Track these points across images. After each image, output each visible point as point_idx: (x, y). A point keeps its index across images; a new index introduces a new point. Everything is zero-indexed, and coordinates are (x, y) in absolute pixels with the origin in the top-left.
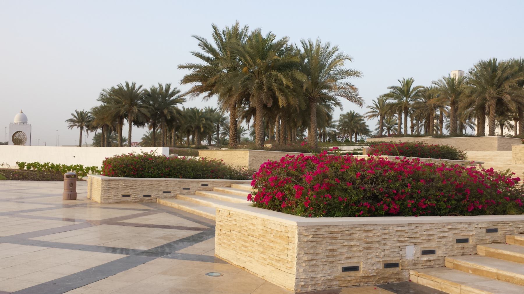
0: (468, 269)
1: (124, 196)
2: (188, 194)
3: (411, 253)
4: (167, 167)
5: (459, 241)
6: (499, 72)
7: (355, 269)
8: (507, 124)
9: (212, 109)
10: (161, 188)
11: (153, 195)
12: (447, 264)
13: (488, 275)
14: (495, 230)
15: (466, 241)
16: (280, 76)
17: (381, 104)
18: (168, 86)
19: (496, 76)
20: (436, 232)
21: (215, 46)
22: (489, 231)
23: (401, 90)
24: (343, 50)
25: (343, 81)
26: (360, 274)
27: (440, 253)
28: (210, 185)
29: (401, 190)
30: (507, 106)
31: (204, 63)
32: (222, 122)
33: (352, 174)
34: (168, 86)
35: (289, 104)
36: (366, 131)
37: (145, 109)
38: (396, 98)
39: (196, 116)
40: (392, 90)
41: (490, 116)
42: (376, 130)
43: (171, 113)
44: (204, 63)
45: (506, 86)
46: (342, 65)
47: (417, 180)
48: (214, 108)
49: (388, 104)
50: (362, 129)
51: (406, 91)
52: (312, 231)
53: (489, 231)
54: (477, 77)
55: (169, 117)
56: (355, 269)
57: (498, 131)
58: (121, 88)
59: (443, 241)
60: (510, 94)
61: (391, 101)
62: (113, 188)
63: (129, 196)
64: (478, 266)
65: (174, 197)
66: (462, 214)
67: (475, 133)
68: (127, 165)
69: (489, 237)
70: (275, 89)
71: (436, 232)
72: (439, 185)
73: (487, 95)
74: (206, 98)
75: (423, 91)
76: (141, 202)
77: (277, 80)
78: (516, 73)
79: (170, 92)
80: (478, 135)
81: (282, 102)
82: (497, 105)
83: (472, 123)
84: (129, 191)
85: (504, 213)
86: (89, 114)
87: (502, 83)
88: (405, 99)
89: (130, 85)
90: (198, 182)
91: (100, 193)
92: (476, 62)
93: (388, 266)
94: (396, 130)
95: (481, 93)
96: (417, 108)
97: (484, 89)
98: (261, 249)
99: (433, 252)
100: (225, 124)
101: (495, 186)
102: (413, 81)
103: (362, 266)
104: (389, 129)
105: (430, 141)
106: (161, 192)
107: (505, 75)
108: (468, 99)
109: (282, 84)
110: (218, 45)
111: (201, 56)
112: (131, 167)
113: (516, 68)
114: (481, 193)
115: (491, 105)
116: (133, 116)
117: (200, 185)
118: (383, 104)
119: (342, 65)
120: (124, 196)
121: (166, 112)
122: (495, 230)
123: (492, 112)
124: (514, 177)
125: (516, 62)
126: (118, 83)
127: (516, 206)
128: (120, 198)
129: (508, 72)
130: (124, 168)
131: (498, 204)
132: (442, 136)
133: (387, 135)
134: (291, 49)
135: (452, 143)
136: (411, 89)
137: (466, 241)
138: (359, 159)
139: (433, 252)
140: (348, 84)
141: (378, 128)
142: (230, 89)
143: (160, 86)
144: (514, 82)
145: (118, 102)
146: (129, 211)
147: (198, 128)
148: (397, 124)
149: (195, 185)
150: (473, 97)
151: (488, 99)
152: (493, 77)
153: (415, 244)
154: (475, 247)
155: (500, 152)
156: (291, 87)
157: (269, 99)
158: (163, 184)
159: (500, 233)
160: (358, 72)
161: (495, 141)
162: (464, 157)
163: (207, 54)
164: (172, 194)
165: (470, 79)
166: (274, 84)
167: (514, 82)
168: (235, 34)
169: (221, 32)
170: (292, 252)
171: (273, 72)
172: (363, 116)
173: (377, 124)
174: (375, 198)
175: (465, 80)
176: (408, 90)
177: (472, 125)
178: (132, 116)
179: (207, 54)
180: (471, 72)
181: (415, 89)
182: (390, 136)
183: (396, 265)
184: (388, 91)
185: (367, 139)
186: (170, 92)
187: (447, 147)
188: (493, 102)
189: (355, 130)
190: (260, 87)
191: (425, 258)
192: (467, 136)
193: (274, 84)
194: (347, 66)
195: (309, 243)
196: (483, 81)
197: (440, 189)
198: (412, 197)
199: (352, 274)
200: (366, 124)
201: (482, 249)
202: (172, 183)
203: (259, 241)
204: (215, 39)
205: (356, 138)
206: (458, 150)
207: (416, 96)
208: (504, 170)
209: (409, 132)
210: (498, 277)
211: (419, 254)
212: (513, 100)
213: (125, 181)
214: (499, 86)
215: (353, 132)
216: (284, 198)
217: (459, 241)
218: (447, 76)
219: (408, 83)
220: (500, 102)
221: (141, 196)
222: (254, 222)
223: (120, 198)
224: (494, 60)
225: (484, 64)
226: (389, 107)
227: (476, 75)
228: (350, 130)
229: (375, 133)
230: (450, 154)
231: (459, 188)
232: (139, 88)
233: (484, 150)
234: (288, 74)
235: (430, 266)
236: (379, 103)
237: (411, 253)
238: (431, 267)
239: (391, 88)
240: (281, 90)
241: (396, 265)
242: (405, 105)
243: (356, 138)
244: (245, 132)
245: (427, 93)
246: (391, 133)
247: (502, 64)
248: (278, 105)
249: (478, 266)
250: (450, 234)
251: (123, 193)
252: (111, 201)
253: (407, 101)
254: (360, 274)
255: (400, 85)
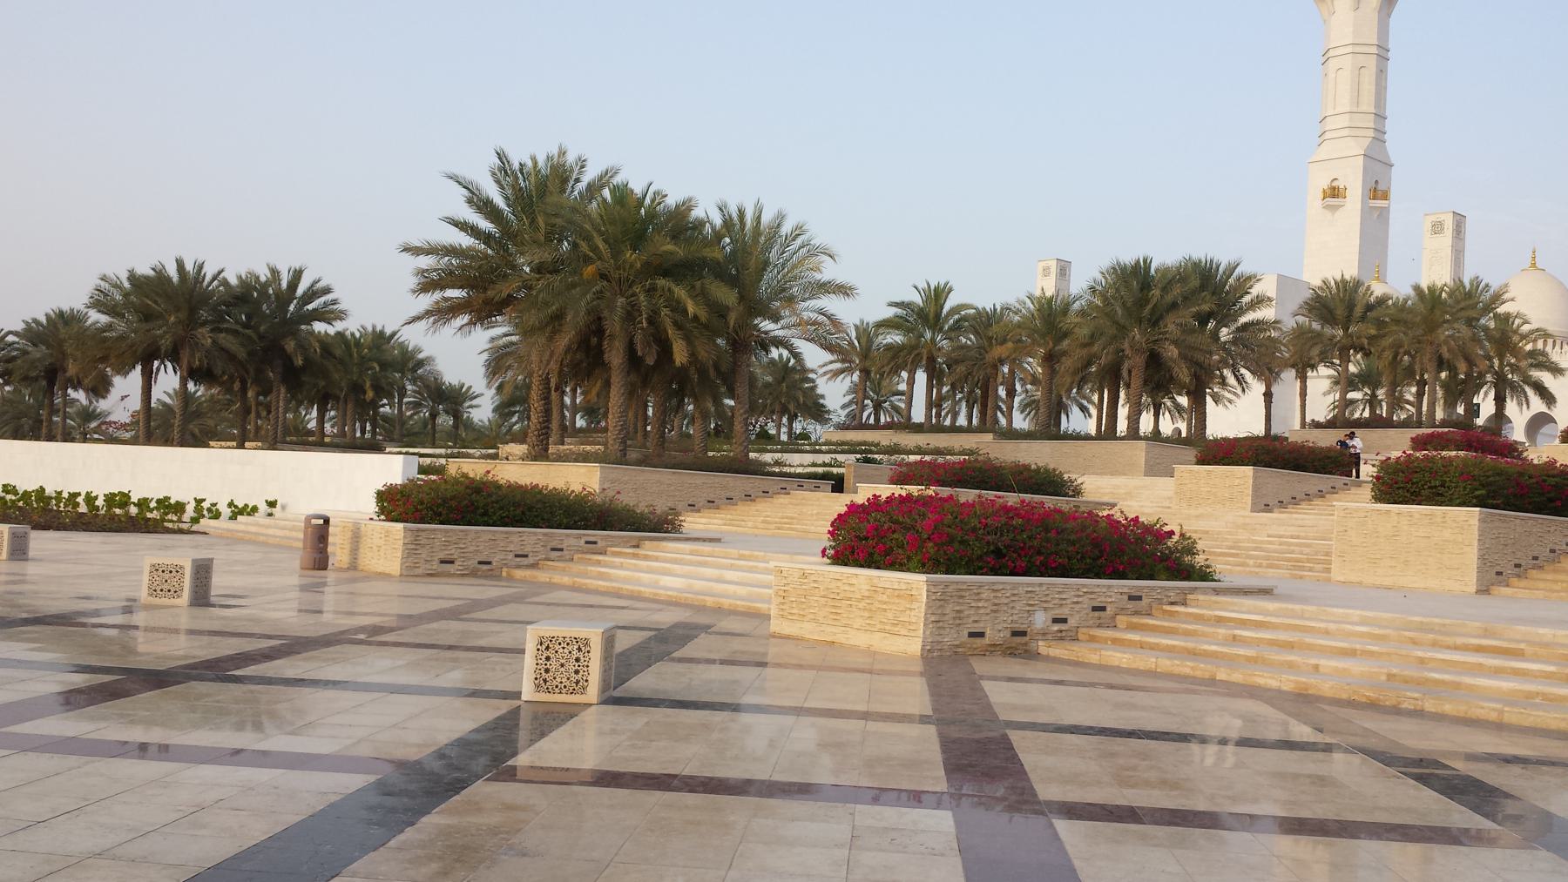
0: (1106, 640)
1: (442, 562)
2: (560, 559)
3: (1040, 620)
4: (517, 505)
5: (1095, 609)
6: (1156, 292)
7: (982, 635)
8: (1169, 403)
9: (382, 333)
10: (511, 547)
11: (496, 560)
12: (1081, 636)
13: (1131, 644)
14: (1139, 598)
15: (1103, 609)
16: (680, 292)
17: (864, 340)
18: (297, 275)
19: (1147, 301)
20: (1070, 596)
21: (500, 202)
22: (1131, 598)
23: (921, 314)
24: (819, 234)
25: (810, 308)
26: (986, 641)
27: (1072, 622)
28: (601, 544)
29: (1029, 544)
30: (1170, 370)
31: (465, 241)
32: (414, 370)
33: (974, 522)
34: (297, 275)
35: (693, 355)
36: (817, 411)
37: (230, 338)
38: (908, 331)
39: (351, 355)
40: (899, 311)
41: (1132, 391)
42: (844, 407)
43: (302, 347)
44: (465, 241)
45: (1171, 325)
46: (818, 270)
47: (1047, 530)
48: (388, 332)
49: (889, 347)
50: (810, 404)
51: (931, 316)
52: (939, 589)
53: (1131, 598)
54: (1105, 299)
55: (299, 362)
56: (982, 635)
57: (1146, 423)
58: (160, 276)
59: (1077, 607)
60: (1175, 343)
61: (895, 338)
62: (423, 546)
63: (452, 562)
64: (1118, 635)
65: (534, 566)
66: (1098, 576)
67: (1091, 427)
68: (445, 501)
69: (1131, 605)
70: (668, 323)
71: (1070, 596)
72: (1073, 537)
73: (1126, 346)
74: (467, 329)
75: (974, 318)
76: (473, 574)
77: (678, 308)
78: (1194, 292)
79: (300, 291)
80: (1100, 437)
81: (680, 355)
82: (1147, 366)
83: (1084, 397)
84: (453, 552)
85: (1151, 578)
86: (10, 338)
87: (1161, 317)
88: (928, 335)
89: (189, 267)
90: (579, 537)
91: (399, 554)
92: (1106, 262)
93: (1015, 634)
94: (896, 409)
95: (1114, 338)
96: (957, 362)
97: (1123, 330)
98: (866, 614)
99: (1064, 621)
100: (421, 377)
101: (1140, 540)
102: (950, 290)
103: (988, 632)
104: (878, 407)
105: (987, 446)
106: (511, 556)
107: (1169, 298)
108: (1085, 352)
109: (685, 311)
110: (507, 198)
111: (456, 224)
112: (454, 504)
113: (1195, 282)
114: (1122, 550)
115: (1134, 364)
116: (198, 355)
117: (582, 542)
118: (870, 341)
119: (818, 270)
120: (442, 562)
121: (290, 345)
122: (1139, 598)
123: (1136, 382)
124: (1166, 529)
125: (1197, 265)
126: (154, 262)
127: (1167, 569)
128: (435, 566)
129: (1177, 291)
130: (439, 506)
131: (1144, 565)
132: (1012, 434)
133: (872, 421)
134: (700, 224)
135: (1037, 455)
136: (945, 311)
137: (1103, 609)
138: (962, 500)
139: (1064, 621)
140: (821, 312)
141: (851, 402)
142: (558, 317)
143: (275, 272)
144: (1186, 316)
145: (147, 316)
146: (162, 624)
147: (357, 389)
148: (902, 393)
149: (573, 541)
150: (1095, 348)
151: (1128, 352)
152: (1142, 302)
153: (1045, 609)
154: (1113, 618)
155: (1149, 480)
156: (703, 320)
157: (649, 344)
158: (515, 539)
159: (1145, 601)
160: (851, 288)
161: (1139, 450)
162: (1077, 492)
163: (485, 225)
164: (530, 560)
165: (1090, 303)
166: (665, 311)
167: (1186, 316)
168: (560, 174)
169: (516, 166)
170: (918, 612)
171: (661, 282)
172: (812, 371)
173: (848, 393)
174: (998, 553)
175: (1076, 306)
176: (938, 315)
177: (1085, 403)
178: (193, 355)
179: (485, 225)
180: (1093, 290)
181: (954, 311)
182: (877, 426)
183: (1024, 634)
184: (891, 312)
185: (818, 431)
186: (300, 291)
187: (1047, 470)
188: (1140, 361)
189: (791, 407)
190: (630, 315)
191: (1056, 627)
192: (1077, 437)
193: (665, 311)
194: (829, 272)
195: (938, 601)
196: (1120, 312)
197: (1073, 543)
198: (1039, 553)
199: (978, 641)
200: (819, 391)
201: (1122, 620)
202: (530, 538)
203: (861, 605)
204: (498, 182)
205: (790, 428)
206: (1066, 476)
207: (957, 327)
208: (1153, 520)
209: (918, 415)
210: (1142, 645)
211: (1049, 622)
212: (1182, 356)
213: (447, 531)
214: (1155, 321)
215: (784, 410)
216: (888, 552)
217: (1095, 609)
218: (1038, 293)
219: (938, 295)
220: (1154, 361)
221: (473, 563)
222: (853, 581)
223: (435, 566)
224: (1145, 261)
225: (1124, 269)
226: (890, 354)
227: (1103, 295)
228: (777, 408)
229: (840, 416)
230: (1051, 483)
231: (1096, 543)
232: (214, 279)
233: (1114, 473)
234: (693, 287)
235: (1061, 637)
236: (858, 338)
237: (1040, 620)
238: (1062, 639)
239: (896, 305)
240: (678, 326)
241: (1024, 634)
242: (930, 352)
243: (790, 428)
244: (474, 402)
245: (984, 323)
246: (882, 420)
247: (1164, 271)
248: (672, 361)
249: (1118, 635)
250: (1085, 599)
251: (442, 556)
252: (419, 571)
253: (933, 340)
254: (986, 641)
255: (917, 299)
